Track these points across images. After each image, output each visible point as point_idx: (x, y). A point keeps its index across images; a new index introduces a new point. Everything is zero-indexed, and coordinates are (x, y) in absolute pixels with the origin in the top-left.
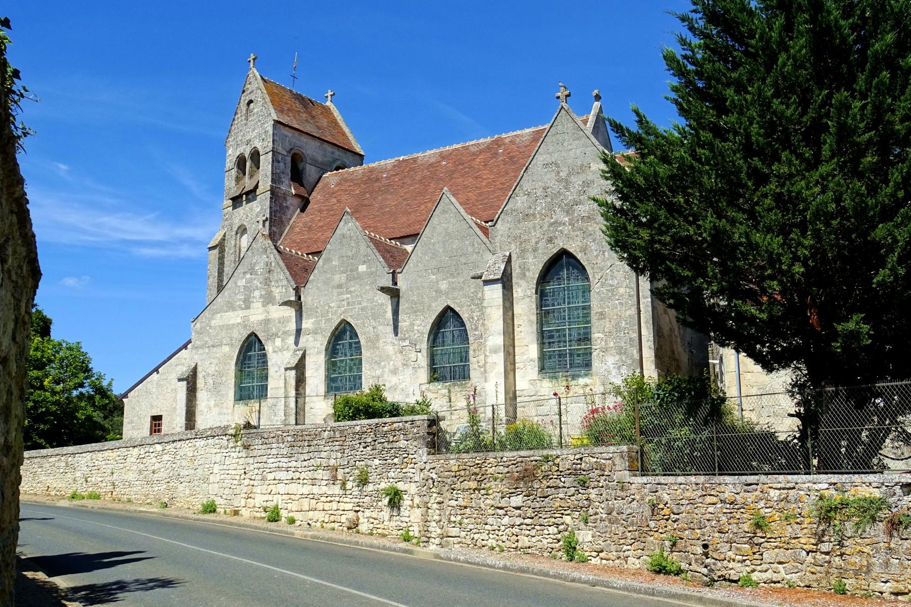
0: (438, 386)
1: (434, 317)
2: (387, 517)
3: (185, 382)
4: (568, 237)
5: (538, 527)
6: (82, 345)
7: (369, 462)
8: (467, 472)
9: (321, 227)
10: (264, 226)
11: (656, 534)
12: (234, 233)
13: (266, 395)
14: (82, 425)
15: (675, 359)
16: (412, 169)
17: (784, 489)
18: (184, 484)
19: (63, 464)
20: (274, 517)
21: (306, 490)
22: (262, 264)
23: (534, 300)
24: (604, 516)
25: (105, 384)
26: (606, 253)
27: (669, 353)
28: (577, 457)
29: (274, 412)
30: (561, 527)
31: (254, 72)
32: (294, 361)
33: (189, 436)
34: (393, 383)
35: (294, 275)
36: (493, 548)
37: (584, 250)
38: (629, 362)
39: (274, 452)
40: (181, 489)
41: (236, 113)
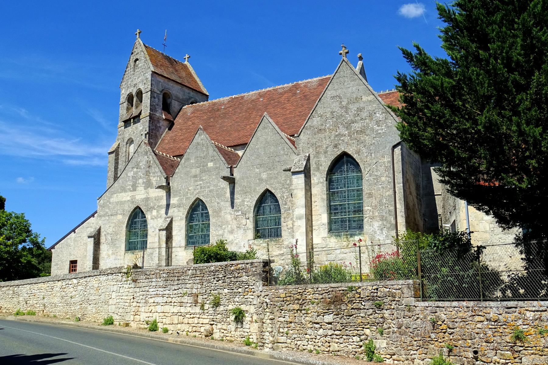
0: (260, 241)
1: (258, 196)
2: (233, 329)
3: (93, 239)
4: (347, 144)
5: (344, 337)
6: (25, 215)
7: (221, 291)
8: (292, 298)
9: (182, 139)
10: (146, 137)
11: (436, 343)
12: (125, 143)
13: (146, 247)
14: (25, 267)
15: (416, 225)
16: (240, 103)
17: (537, 311)
18: (92, 306)
19: (11, 292)
20: (154, 328)
21: (176, 310)
22: (144, 162)
23: (325, 185)
24: (396, 329)
25: (40, 240)
26: (373, 154)
27: (413, 220)
28: (374, 287)
29: (152, 257)
30: (363, 337)
31: (139, 41)
32: (165, 225)
33: (96, 274)
34: (231, 239)
35: (165, 169)
36: (311, 351)
37: (358, 152)
38: (388, 225)
39: (154, 284)
40: (90, 309)
41: (127, 67)
